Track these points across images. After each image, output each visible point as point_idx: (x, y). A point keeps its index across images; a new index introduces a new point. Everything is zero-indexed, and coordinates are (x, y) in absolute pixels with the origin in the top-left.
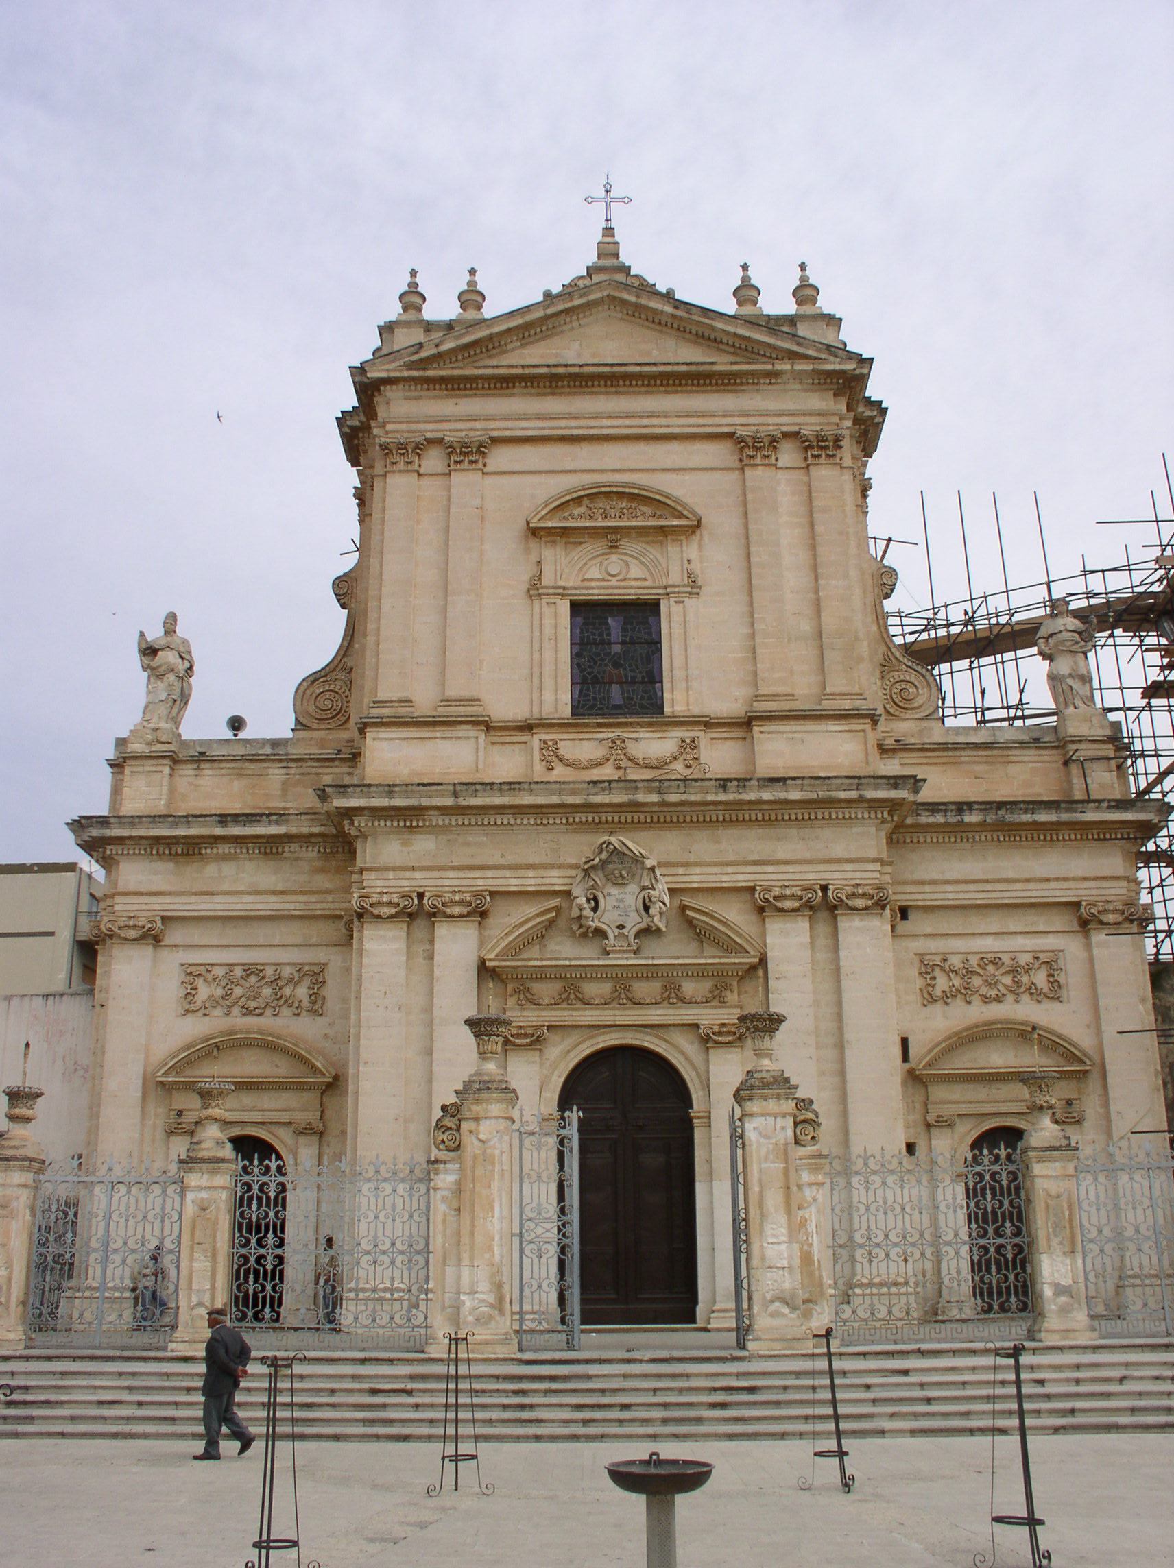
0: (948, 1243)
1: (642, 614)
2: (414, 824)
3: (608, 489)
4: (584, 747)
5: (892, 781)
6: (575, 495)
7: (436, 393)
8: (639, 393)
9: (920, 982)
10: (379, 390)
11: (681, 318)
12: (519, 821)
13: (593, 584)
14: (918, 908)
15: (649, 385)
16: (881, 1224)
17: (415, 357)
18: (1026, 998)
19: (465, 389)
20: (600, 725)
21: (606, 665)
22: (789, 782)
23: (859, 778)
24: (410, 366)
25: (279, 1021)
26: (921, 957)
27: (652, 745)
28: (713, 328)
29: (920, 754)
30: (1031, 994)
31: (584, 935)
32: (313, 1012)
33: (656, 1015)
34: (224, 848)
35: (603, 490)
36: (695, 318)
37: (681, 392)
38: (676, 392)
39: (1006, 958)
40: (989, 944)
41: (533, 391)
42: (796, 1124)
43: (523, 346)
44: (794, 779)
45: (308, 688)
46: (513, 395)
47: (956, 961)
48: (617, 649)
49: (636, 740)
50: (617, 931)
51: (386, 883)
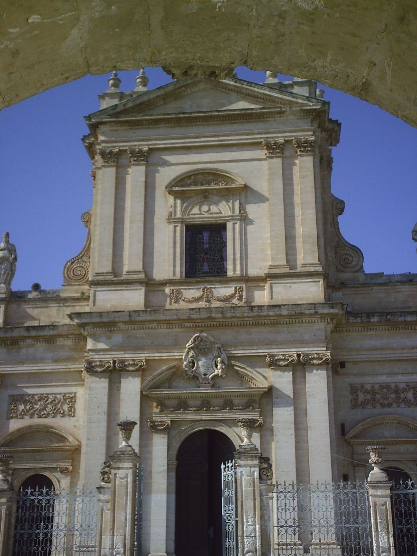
0: (315, 526)
1: (218, 229)
2: (115, 329)
3: (203, 171)
4: (192, 293)
5: (331, 305)
6: (187, 175)
7: (125, 128)
8: (219, 124)
9: (350, 397)
10: (98, 127)
11: (238, 87)
12: (159, 327)
13: (196, 216)
14: (350, 362)
15: (223, 120)
16: (284, 517)
17: (115, 111)
18: (403, 405)
19: (138, 125)
20: (197, 282)
21: (201, 254)
22: (282, 307)
23: (315, 304)
24: (112, 116)
25: (54, 420)
26: (351, 385)
27: (224, 291)
28: (254, 91)
29: (352, 289)
30: (405, 403)
31: (189, 378)
32: (70, 415)
33: (219, 416)
34: (29, 341)
35: (201, 172)
36: (245, 86)
37: (238, 123)
38: (236, 123)
39: (393, 386)
40: (383, 379)
41: (169, 125)
42: (260, 470)
43: (165, 104)
44: (284, 305)
45: (70, 266)
46: (160, 127)
47: (368, 387)
48: (206, 246)
49: (214, 288)
50: (203, 376)
51: (100, 357)
